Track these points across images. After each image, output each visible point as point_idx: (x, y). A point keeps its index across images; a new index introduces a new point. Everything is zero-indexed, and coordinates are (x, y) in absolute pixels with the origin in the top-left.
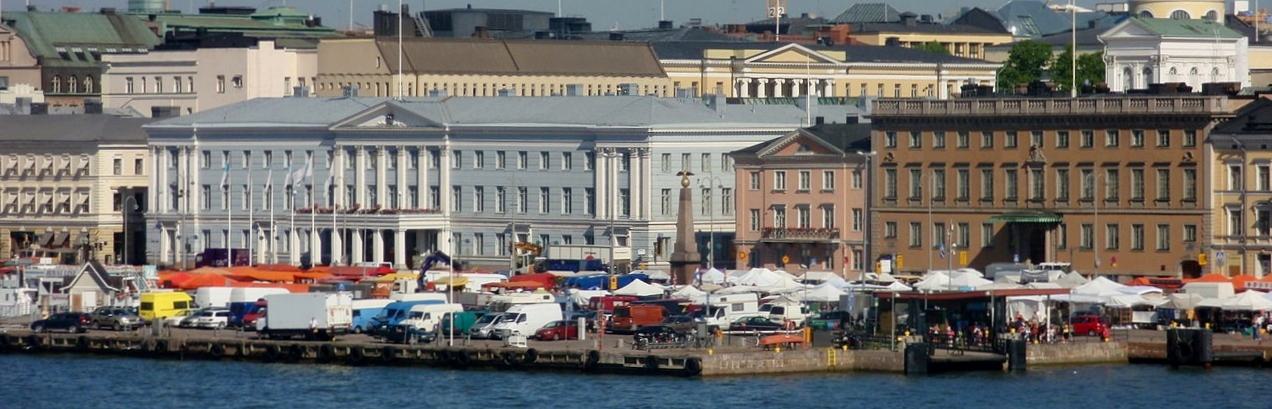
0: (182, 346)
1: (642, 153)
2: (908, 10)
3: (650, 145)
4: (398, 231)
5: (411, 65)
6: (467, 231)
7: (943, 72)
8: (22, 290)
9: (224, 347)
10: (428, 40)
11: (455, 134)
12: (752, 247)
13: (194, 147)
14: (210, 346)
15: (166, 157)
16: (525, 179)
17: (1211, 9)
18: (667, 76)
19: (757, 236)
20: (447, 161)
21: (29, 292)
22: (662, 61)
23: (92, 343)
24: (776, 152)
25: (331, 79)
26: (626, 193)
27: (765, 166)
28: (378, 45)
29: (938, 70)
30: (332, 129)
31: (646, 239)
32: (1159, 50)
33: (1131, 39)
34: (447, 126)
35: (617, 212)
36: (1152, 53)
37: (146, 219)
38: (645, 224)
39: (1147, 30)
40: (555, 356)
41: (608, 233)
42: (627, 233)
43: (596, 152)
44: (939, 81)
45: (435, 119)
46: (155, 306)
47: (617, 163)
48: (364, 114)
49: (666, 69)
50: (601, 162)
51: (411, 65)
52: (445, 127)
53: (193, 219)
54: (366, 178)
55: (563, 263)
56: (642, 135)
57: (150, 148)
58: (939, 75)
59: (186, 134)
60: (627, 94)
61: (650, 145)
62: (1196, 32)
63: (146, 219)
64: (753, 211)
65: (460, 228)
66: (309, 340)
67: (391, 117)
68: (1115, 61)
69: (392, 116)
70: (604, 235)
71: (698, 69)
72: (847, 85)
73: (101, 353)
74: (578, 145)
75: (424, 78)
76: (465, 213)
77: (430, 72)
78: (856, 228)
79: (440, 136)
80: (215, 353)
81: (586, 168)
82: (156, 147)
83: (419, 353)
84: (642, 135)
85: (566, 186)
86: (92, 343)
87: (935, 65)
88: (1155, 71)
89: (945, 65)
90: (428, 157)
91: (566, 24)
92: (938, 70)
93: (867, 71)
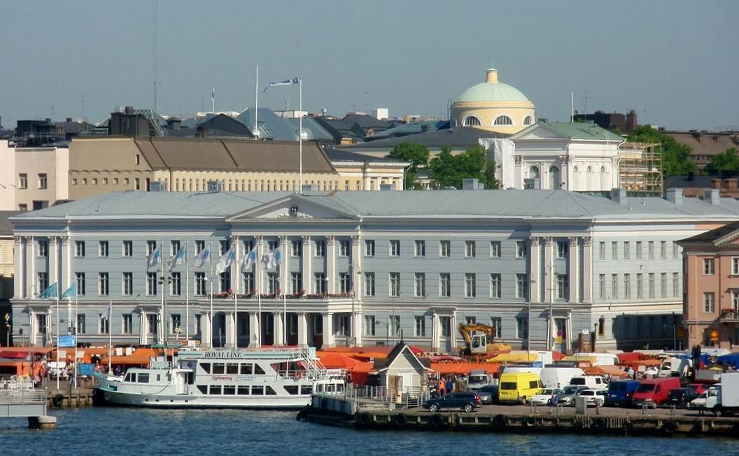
0: (627, 423)
1: (582, 242)
2: (174, 116)
3: (591, 234)
4: (327, 314)
5: (165, 164)
6: (382, 314)
7: (368, 170)
8: (175, 371)
9: (677, 423)
10: (163, 139)
11: (366, 226)
12: (706, 327)
13: (67, 237)
14: (661, 424)
15: (34, 248)
16: (397, 265)
17: (525, 117)
18: (336, 173)
19: (712, 317)
20: (359, 250)
21: (180, 372)
22: (334, 163)
23: (510, 421)
24: (734, 240)
25: (85, 175)
26: (564, 279)
27: (720, 253)
28: (136, 143)
29: (364, 168)
30: (229, 220)
31: (589, 320)
32: (568, 150)
33: (547, 141)
34: (361, 217)
35: (553, 297)
36: (560, 153)
37: (11, 304)
38: (589, 307)
39: (555, 134)
40: (479, 419)
41: (545, 315)
42: (568, 315)
43: (530, 240)
44: (364, 177)
45: (352, 212)
46: (518, 385)
47: (552, 250)
48: (260, 209)
49: (337, 170)
50: (536, 251)
51: (165, 164)
52: (360, 219)
53: (67, 304)
54: (36, 265)
55: (320, 334)
56: (585, 225)
57: (16, 239)
58: (364, 173)
59: (60, 225)
60: (533, 188)
61: (591, 234)
62: (593, 135)
63: (11, 304)
64: (707, 294)
65: (371, 312)
66: (724, 416)
67: (294, 209)
68: (522, 160)
69: (297, 208)
70: (541, 316)
71: (360, 170)
72: (347, 182)
73: (617, 433)
74: (509, 235)
75: (177, 174)
76: (379, 297)
77: (181, 169)
78: (707, 310)
79: (352, 227)
80: (599, 428)
81: (517, 256)
82: (23, 238)
83: (419, 420)
84: (585, 225)
85: (127, 271)
86: (510, 421)
87: (362, 164)
88: (564, 169)
89: (370, 164)
90: (337, 246)
91: (34, 126)
92: (364, 168)
93: (349, 170)
